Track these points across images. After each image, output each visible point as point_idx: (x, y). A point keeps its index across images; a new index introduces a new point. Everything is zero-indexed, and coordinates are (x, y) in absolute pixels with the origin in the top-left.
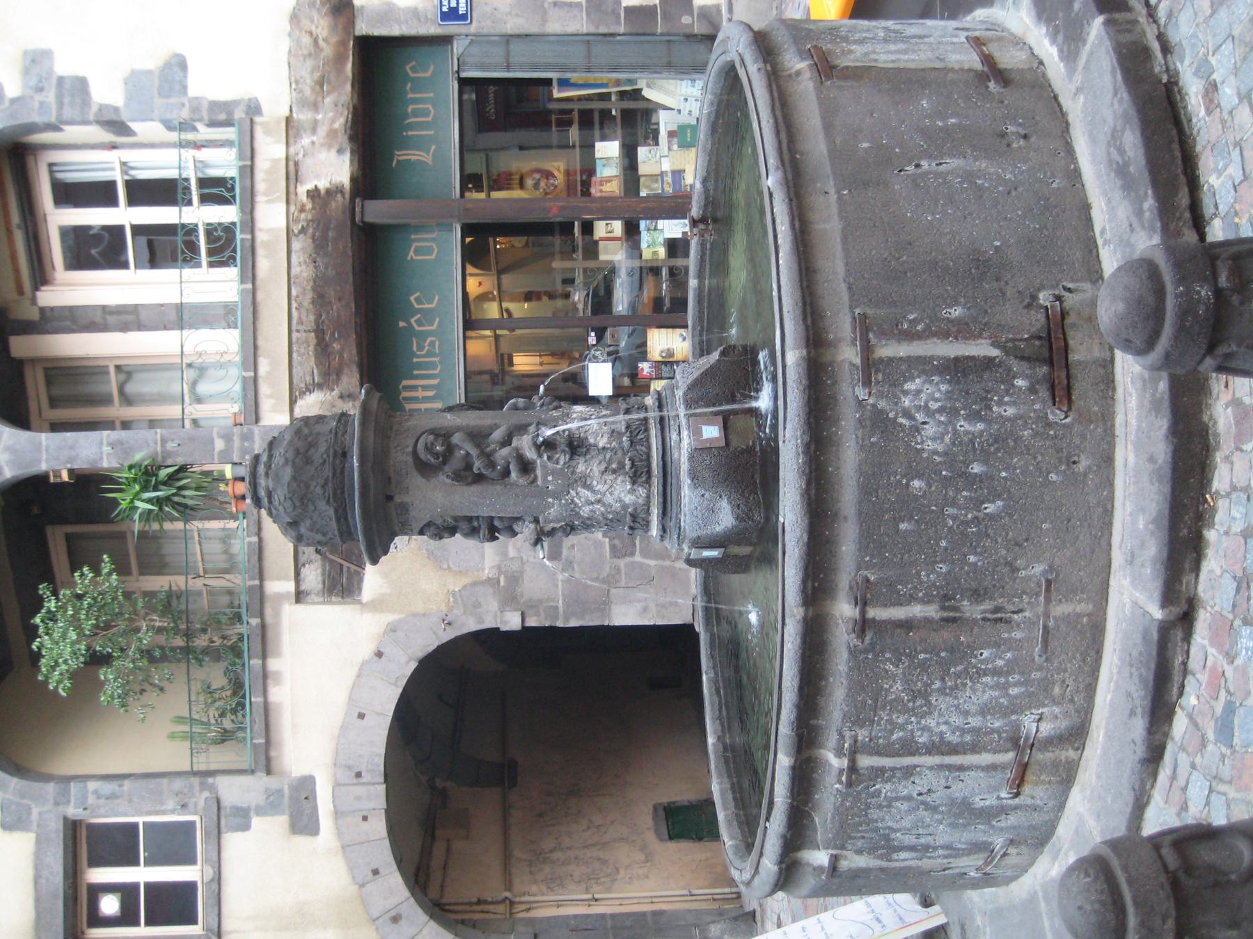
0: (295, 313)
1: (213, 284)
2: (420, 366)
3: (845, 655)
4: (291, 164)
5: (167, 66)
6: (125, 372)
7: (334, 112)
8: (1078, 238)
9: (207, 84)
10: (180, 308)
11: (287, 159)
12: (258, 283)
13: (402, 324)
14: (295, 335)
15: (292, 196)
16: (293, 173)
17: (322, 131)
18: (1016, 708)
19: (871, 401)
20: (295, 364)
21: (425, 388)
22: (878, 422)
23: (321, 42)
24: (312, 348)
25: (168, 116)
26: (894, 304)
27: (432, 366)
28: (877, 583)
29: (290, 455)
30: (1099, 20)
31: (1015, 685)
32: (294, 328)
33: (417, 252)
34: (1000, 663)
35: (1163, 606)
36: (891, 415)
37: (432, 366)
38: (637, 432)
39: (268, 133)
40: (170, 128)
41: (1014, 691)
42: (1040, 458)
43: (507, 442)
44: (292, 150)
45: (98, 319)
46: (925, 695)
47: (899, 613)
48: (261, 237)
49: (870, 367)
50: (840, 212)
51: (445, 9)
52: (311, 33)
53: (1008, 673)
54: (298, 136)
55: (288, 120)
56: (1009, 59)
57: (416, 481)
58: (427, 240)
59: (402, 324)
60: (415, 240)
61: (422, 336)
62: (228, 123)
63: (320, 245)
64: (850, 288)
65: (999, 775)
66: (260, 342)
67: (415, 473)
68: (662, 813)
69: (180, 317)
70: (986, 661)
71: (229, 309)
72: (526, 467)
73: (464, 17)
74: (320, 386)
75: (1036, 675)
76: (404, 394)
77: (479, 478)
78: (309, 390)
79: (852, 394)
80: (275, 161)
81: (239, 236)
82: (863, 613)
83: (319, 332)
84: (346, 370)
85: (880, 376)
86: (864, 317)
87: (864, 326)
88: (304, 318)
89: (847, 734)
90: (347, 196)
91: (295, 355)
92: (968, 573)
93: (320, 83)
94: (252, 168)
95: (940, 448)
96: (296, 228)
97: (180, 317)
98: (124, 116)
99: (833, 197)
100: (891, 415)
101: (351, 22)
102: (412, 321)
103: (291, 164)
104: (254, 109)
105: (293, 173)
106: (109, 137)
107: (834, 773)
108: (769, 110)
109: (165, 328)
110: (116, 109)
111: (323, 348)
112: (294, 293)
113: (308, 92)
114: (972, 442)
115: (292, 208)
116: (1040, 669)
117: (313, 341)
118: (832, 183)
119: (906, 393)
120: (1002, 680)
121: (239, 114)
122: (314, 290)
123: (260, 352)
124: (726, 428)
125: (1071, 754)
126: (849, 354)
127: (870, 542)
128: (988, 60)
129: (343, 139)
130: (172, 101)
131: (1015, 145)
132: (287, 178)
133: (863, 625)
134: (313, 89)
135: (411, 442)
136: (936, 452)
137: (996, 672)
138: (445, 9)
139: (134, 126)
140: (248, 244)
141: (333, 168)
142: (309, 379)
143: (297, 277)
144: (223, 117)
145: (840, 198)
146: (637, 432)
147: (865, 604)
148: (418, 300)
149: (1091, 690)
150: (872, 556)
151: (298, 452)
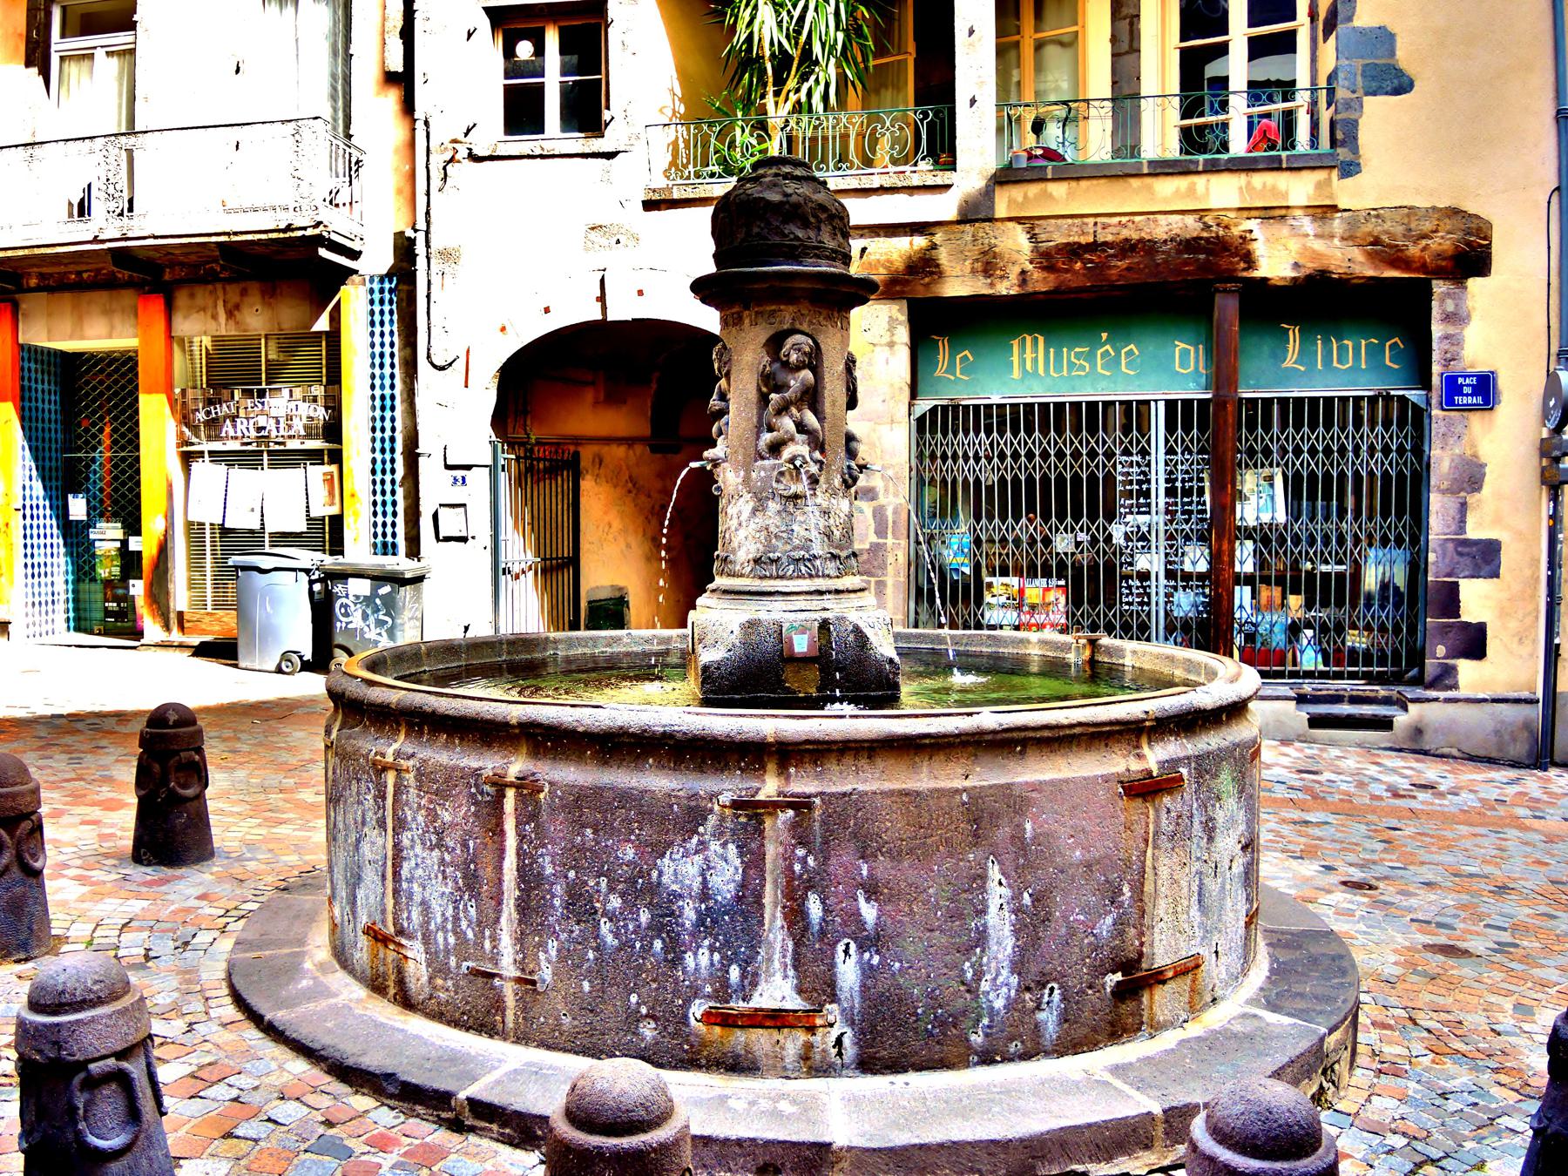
0: (1115, 220)
1: (1161, 131)
2: (1058, 355)
3: (475, 765)
4: (1283, 212)
5: (1399, 73)
6: (1071, 43)
7: (1345, 258)
8: (905, 1056)
9: (1379, 119)
10: (1136, 96)
11: (1288, 207)
12: (1148, 180)
13: (1104, 335)
14: (1091, 221)
15: (1245, 214)
16: (1272, 214)
17: (1318, 245)
18: (427, 939)
19: (716, 808)
20: (1059, 221)
21: (1035, 360)
22: (694, 816)
23: (1424, 242)
24: (1076, 239)
25: (1341, 75)
26: (826, 842)
27: (1058, 368)
28: (537, 802)
29: (794, 198)
30: (1157, 1110)
31: (445, 939)
32: (1099, 220)
33: (1185, 353)
34: (464, 924)
35: (468, 1099)
36: (701, 829)
37: (1058, 368)
38: (804, 563)
39: (1319, 186)
40: (1330, 79)
41: (440, 936)
42: (654, 986)
43: (801, 427)
44: (1298, 213)
45: (1125, 11)
46: (440, 845)
47: (510, 825)
48: (1200, 181)
49: (752, 811)
50: (937, 790)
51: (1460, 380)
52: (1436, 231)
53: (455, 933)
54: (1314, 218)
55: (1334, 208)
56: (1162, 1001)
57: (761, 334)
58: (1197, 362)
59: (1104, 335)
60: (1197, 351)
61: (1090, 357)
62: (1334, 143)
63: (1190, 245)
64: (844, 794)
65: (378, 918)
66: (1084, 183)
67: (771, 332)
68: (618, 595)
69: (1125, 95)
70: (466, 910)
71: (1135, 150)
72: (775, 449)
73: (1450, 402)
74: (1035, 250)
75: (453, 961)
76: (1029, 339)
77: (764, 400)
78: (1033, 237)
79: (727, 787)
80: (1285, 195)
81: (1201, 158)
82: (511, 785)
83: (1094, 246)
84: (1052, 277)
85: (743, 820)
86: (809, 806)
87: (801, 805)
88: (1110, 230)
89: (411, 763)
90: (1245, 274)
91: (1070, 221)
92: (543, 898)
93: (1376, 241)
94: (1280, 169)
95: (665, 879)
96: (1209, 220)
97: (1125, 95)
98: (1341, 27)
99: (959, 783)
100: (701, 829)
101: (1442, 274)
102: (1108, 347)
103: (1283, 212)
104: (1349, 169)
105: (1272, 214)
106: (1322, 14)
107: (383, 749)
108: (1083, 720)
109: (1114, 83)
110: (1350, 19)
111: (1073, 251)
112: (1137, 219)
113: (1369, 227)
114: (672, 914)
115: (1232, 215)
116: (459, 966)
117: (1083, 240)
118: (977, 784)
119: (724, 845)
120: (449, 926)
121: (1343, 153)
122: (1141, 240)
123: (1073, 184)
124: (805, 660)
125: (392, 991)
126: (770, 787)
127: (579, 802)
128: (1158, 978)
129: (1310, 266)
130: (1359, 78)
131: (1028, 996)
132: (1265, 208)
133: (500, 786)
134: (1370, 234)
135: (805, 327)
136: (661, 874)
137: (456, 919)
138: (1460, 380)
139: (1332, 38)
140: (1192, 167)
141: (1276, 259)
142: (1043, 237)
143: (1155, 221)
144: (1339, 136)
145: (957, 791)
146: (804, 563)
147: (518, 787)
148: (1130, 353)
149: (438, 1016)
150: (561, 799)
151: (797, 206)
